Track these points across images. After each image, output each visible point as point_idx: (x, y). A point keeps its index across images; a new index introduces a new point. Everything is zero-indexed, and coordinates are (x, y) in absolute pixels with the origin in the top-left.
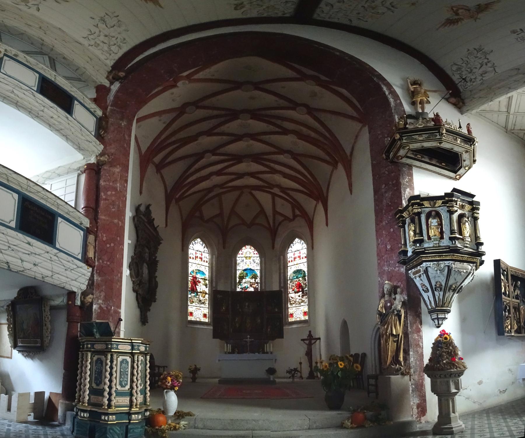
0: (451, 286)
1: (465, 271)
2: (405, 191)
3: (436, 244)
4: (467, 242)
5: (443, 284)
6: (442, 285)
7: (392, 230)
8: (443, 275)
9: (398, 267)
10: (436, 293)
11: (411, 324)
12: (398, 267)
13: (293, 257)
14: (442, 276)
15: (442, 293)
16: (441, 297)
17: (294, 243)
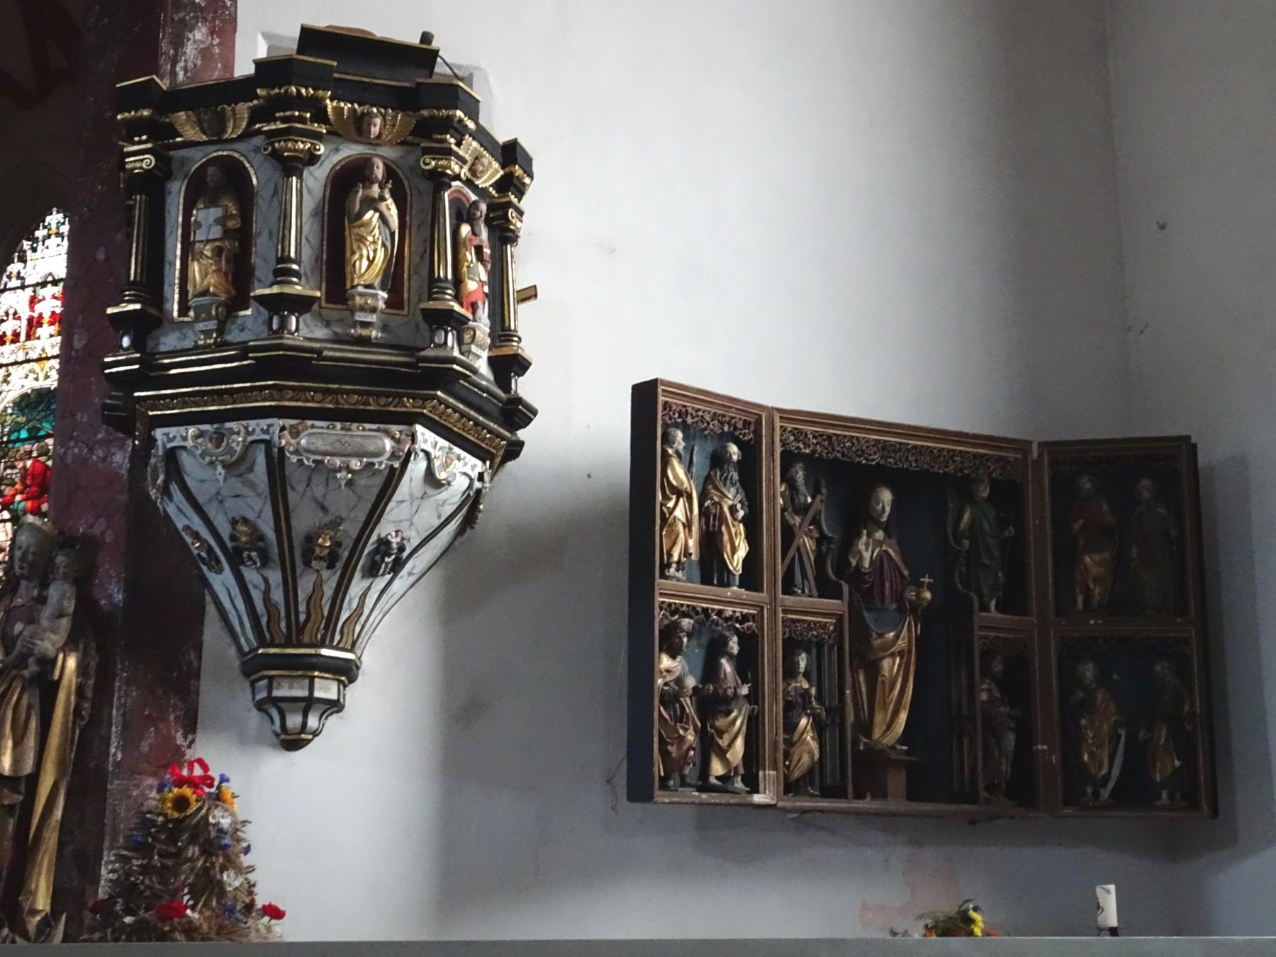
0: (310, 539)
1: (356, 464)
2: (179, 43)
3: (207, 333)
4: (360, 317)
5: (267, 527)
6: (262, 538)
7: (101, 255)
8: (252, 485)
9: (102, 443)
10: (251, 575)
11: (126, 726)
12: (102, 443)
13: (25, 313)
14: (246, 491)
15: (275, 576)
16: (277, 595)
17: (40, 233)
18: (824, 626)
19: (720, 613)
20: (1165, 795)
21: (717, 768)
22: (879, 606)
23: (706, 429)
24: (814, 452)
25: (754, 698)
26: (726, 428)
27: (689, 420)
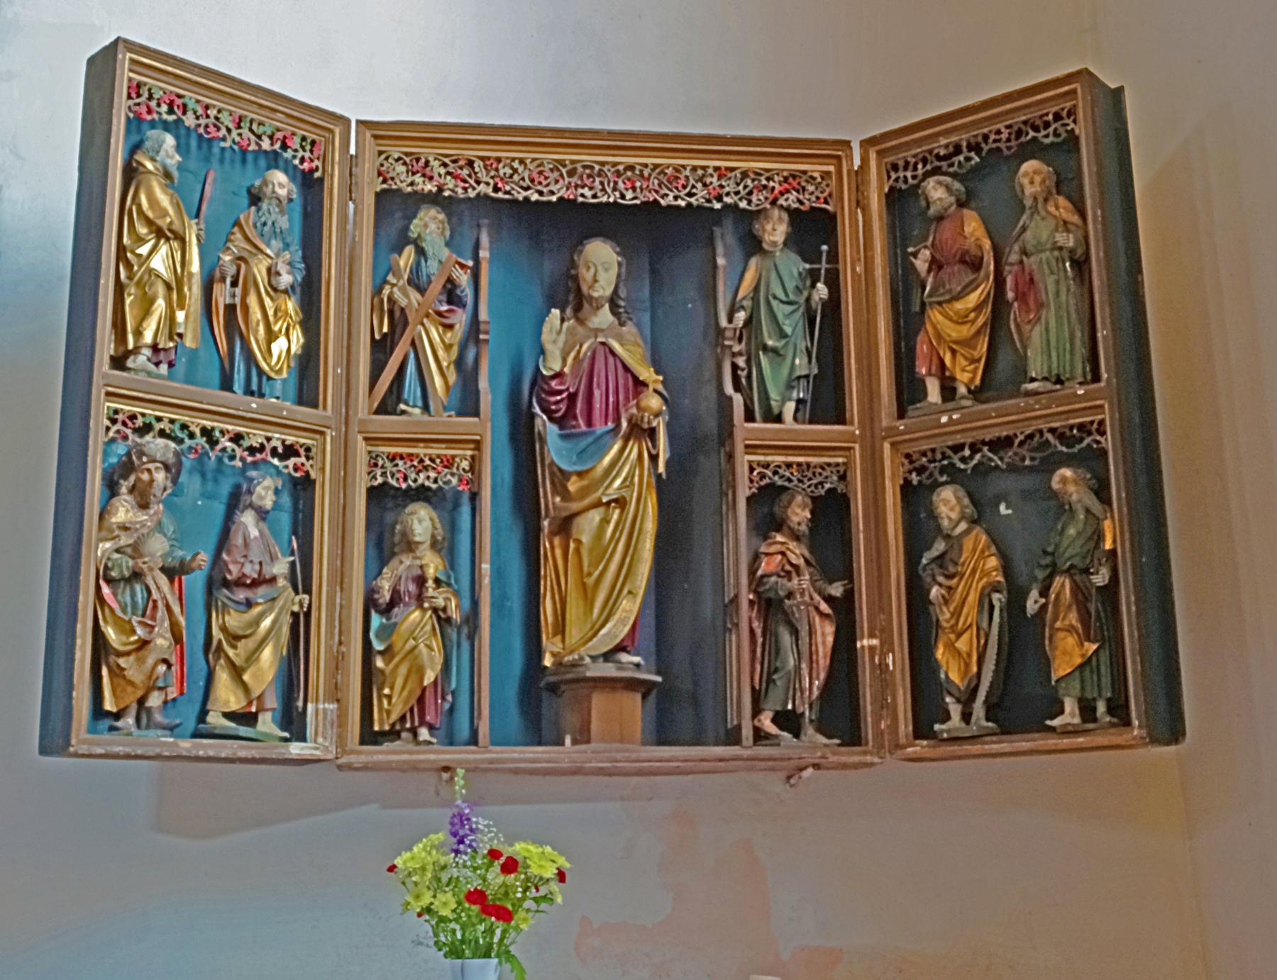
18: (449, 463)
19: (237, 438)
20: (1070, 705)
21: (227, 696)
22: (584, 428)
23: (224, 139)
24: (440, 189)
25: (302, 579)
26: (266, 144)
27: (189, 120)
